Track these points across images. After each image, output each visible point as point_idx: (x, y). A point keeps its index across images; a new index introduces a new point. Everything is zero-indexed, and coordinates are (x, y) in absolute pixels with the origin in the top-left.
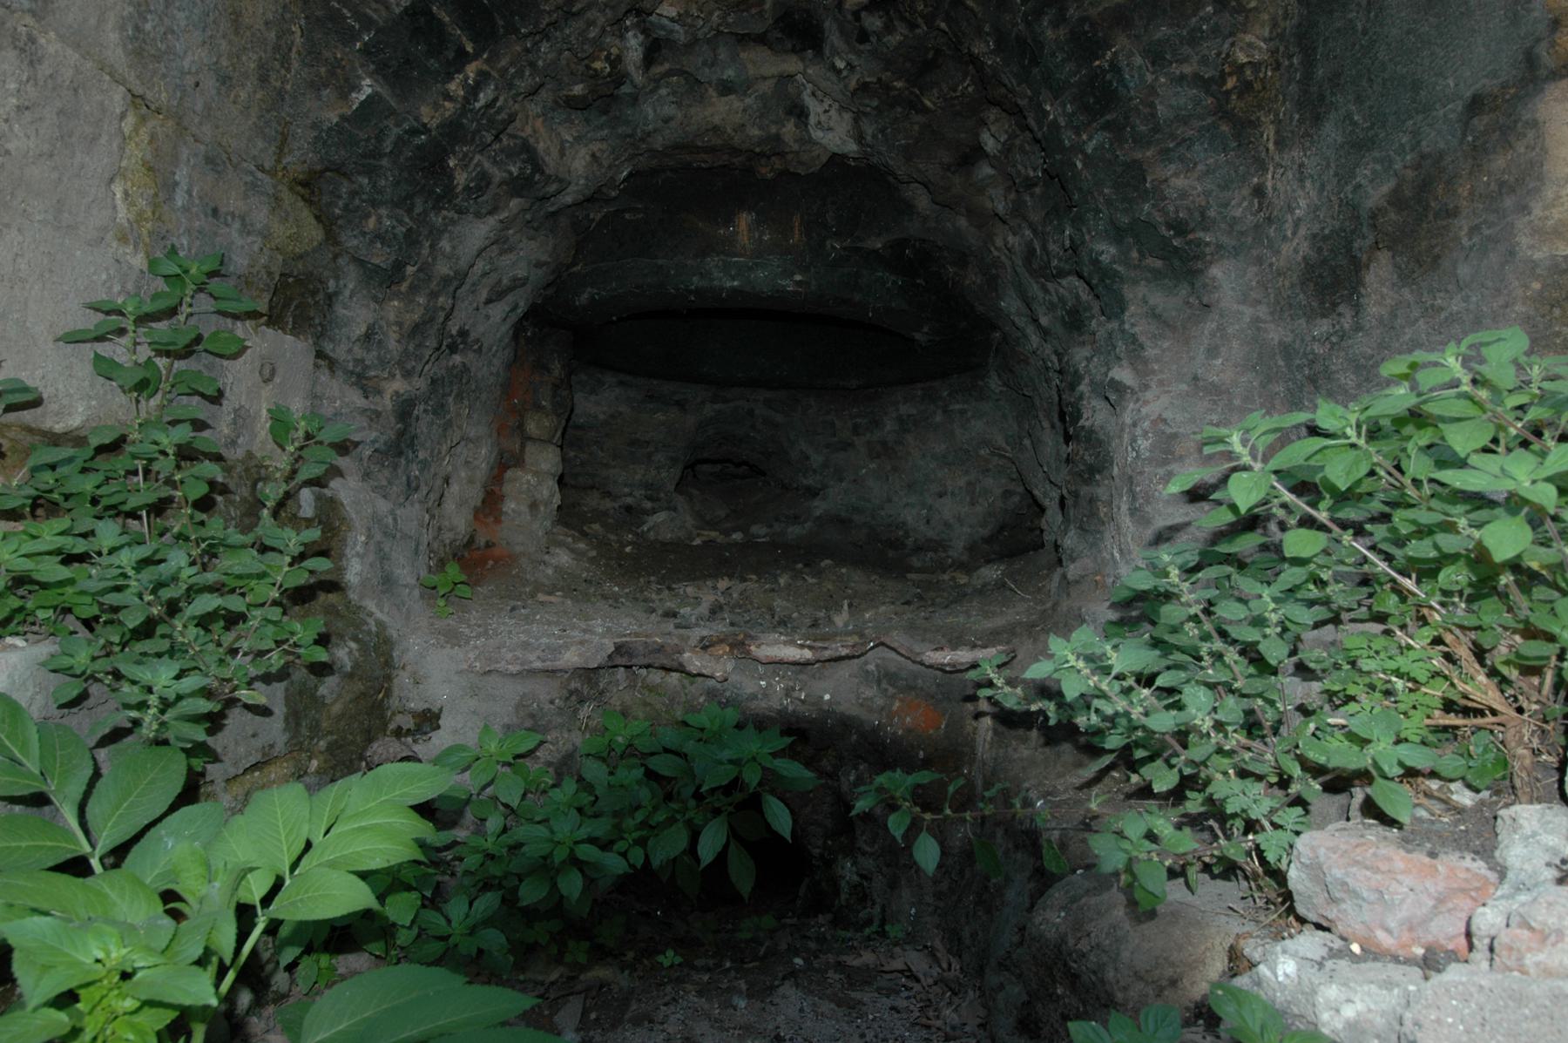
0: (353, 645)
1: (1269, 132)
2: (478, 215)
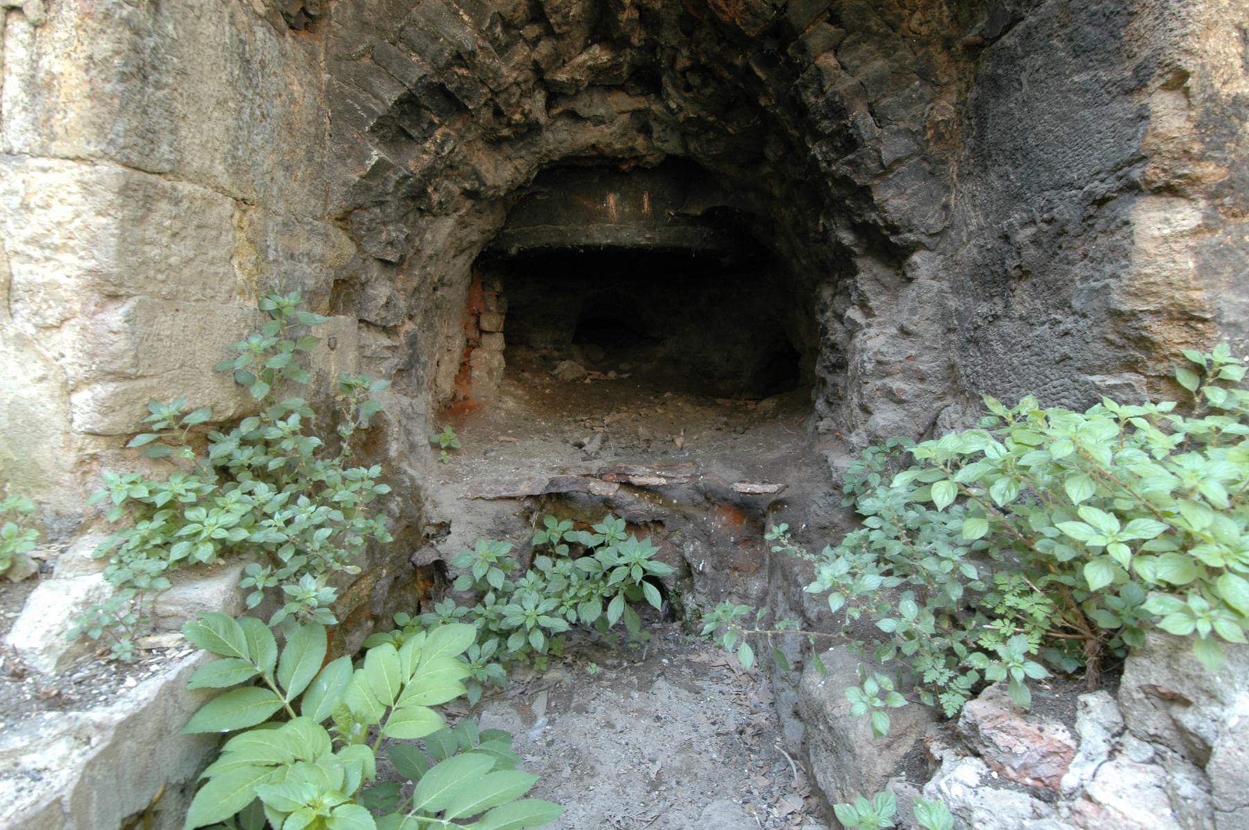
0: (399, 499)
1: (953, 169)
2: (447, 215)
